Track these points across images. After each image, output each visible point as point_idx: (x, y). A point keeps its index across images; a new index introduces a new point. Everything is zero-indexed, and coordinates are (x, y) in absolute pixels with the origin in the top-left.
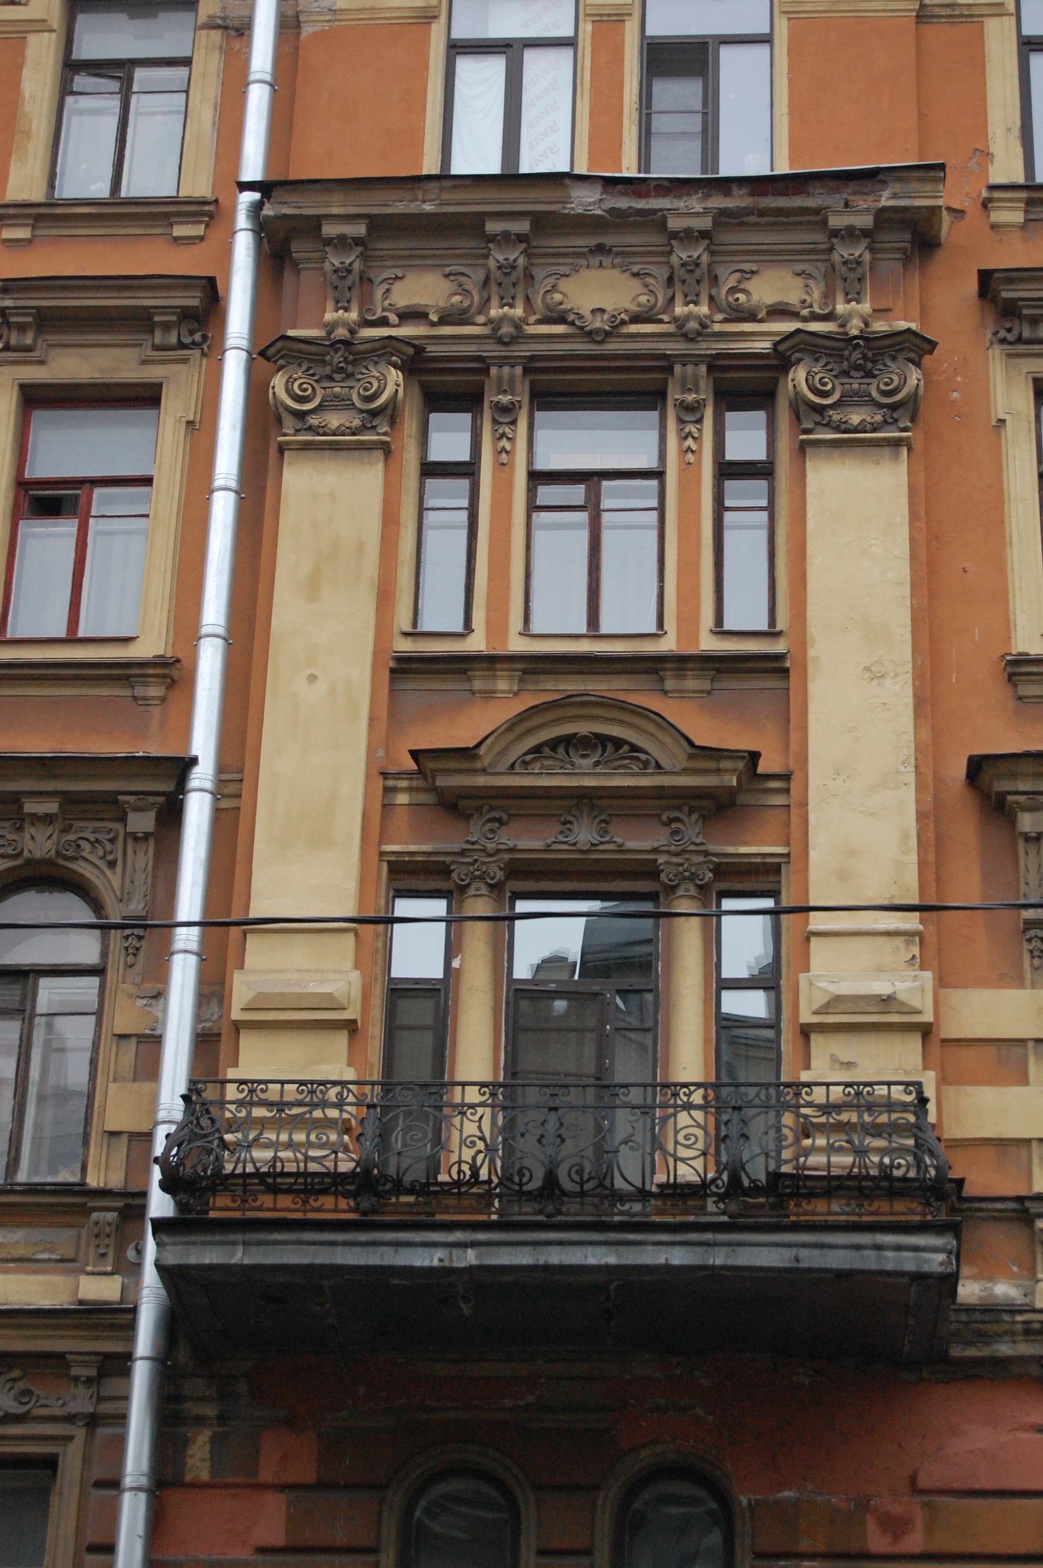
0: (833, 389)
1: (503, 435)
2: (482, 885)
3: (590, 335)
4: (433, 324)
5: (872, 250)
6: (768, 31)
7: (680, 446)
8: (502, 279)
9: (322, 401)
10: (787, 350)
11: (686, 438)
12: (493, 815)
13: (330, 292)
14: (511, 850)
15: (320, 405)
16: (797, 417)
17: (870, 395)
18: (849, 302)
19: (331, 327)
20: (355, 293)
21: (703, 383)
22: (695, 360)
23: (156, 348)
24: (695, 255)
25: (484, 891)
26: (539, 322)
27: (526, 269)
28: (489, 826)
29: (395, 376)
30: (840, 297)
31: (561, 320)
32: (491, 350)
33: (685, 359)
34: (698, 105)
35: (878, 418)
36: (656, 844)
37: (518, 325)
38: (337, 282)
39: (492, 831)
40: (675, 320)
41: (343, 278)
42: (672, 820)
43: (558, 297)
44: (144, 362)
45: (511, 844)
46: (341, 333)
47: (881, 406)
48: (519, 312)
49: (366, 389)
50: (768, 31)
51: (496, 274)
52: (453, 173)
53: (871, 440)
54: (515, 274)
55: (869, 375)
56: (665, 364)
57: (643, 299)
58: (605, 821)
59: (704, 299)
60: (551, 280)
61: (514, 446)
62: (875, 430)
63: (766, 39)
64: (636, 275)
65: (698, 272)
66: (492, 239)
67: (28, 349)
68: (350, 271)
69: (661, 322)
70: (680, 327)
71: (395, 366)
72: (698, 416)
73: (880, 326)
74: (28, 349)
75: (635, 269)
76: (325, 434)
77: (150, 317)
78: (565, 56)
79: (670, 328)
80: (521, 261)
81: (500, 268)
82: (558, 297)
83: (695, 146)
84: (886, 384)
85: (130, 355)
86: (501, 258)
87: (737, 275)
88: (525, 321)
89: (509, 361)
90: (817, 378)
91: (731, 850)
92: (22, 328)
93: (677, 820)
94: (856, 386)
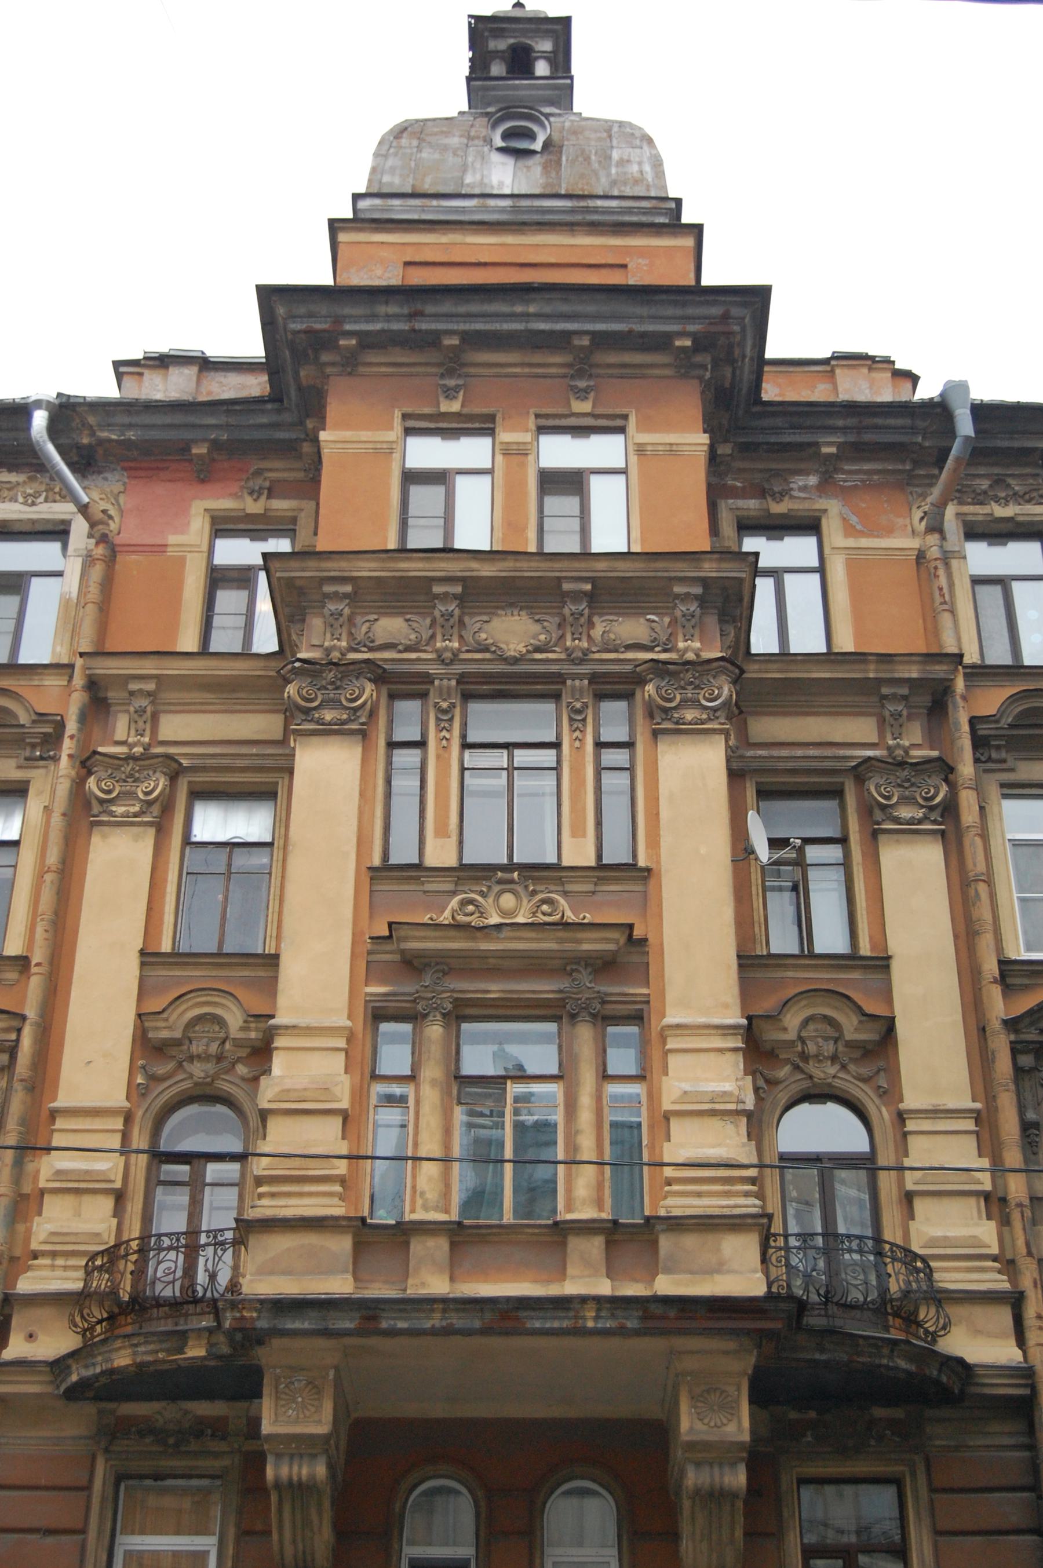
0: (675, 697)
1: (577, 728)
2: (437, 1014)
3: (505, 660)
4: (400, 652)
5: (590, 607)
6: (624, 466)
7: (571, 736)
8: (685, 623)
9: (322, 701)
10: (644, 671)
11: (575, 731)
12: (438, 967)
13: (329, 629)
14: (453, 991)
15: (320, 705)
16: (651, 716)
17: (340, 702)
18: (686, 641)
19: (328, 651)
20: (456, 630)
21: (453, 693)
22: (580, 677)
23: (26, 759)
24: (451, 609)
25: (439, 1017)
26: (468, 651)
27: (460, 617)
28: (436, 975)
29: (369, 687)
30: (680, 637)
31: (486, 649)
32: (566, 668)
33: (574, 677)
34: (577, 512)
35: (345, 716)
36: (562, 987)
37: (586, 652)
38: (333, 622)
39: (438, 978)
40: (437, 651)
41: (337, 619)
42: (573, 970)
43: (483, 636)
44: (19, 767)
45: (452, 986)
46: (335, 655)
47: (706, 708)
48: (456, 645)
49: (351, 694)
50: (624, 466)
51: (440, 620)
52: (593, 551)
53: (698, 729)
54: (341, 619)
55: (697, 687)
56: (560, 678)
57: (542, 637)
58: (443, 971)
59: (455, 637)
60: (478, 625)
61: (451, 735)
62: (702, 724)
63: (623, 472)
64: (538, 621)
65: (452, 621)
66: (437, 596)
67: (1004, 761)
68: (341, 615)
69: (554, 652)
70: (569, 655)
71: (370, 680)
72: (450, 716)
73: (353, 656)
74: (1004, 761)
75: (537, 617)
76: (323, 724)
77: (23, 740)
78: (487, 480)
79: (563, 656)
80: (347, 611)
81: (684, 616)
82: (483, 636)
83: (577, 538)
84: (351, 694)
85: (12, 763)
86: (443, 609)
87: (368, 624)
88: (459, 650)
89: (580, 677)
90: (305, 691)
91: (632, 991)
92: (998, 748)
93: (576, 970)
94: (332, 695)
